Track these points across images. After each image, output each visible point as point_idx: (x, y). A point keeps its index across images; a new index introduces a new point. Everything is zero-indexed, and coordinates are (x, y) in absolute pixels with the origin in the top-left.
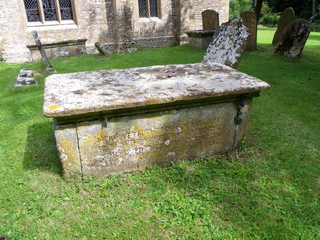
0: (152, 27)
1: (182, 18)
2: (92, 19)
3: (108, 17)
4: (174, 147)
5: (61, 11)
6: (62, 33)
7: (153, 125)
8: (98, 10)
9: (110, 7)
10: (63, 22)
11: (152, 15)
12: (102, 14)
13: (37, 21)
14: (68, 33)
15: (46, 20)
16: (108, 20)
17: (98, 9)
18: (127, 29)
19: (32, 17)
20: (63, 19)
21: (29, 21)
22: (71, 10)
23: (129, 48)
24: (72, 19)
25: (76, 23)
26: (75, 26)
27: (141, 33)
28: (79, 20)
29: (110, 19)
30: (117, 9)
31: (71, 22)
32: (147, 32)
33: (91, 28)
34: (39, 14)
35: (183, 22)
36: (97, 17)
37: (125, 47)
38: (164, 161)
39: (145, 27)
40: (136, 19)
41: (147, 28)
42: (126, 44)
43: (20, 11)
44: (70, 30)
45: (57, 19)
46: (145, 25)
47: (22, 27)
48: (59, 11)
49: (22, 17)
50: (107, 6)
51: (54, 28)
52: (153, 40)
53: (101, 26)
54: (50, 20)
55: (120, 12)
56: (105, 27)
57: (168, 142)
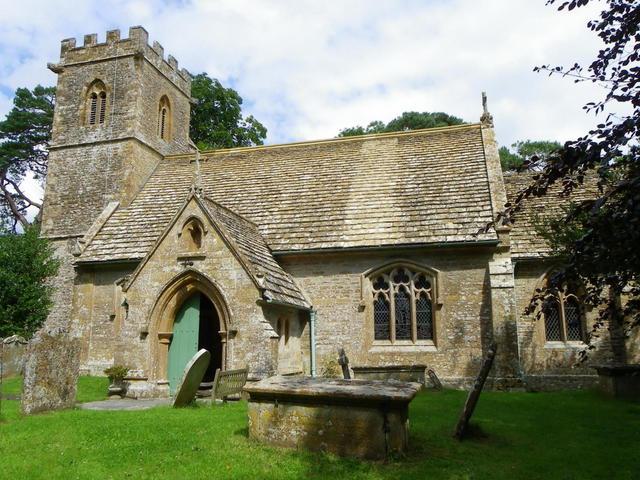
0: (568, 358)
1: (628, 344)
2: (458, 340)
3: (483, 338)
4: (325, 438)
5: (418, 328)
6: (414, 357)
7: (304, 413)
8: (469, 328)
9: (487, 324)
10: (418, 342)
11: (572, 338)
12: (473, 334)
13: (385, 339)
14: (423, 358)
15: (397, 338)
16: (483, 343)
17: (469, 326)
18: (508, 359)
19: (380, 335)
20: (419, 338)
21: (376, 339)
22: (431, 326)
23: (513, 387)
24: (432, 338)
25: (436, 345)
26: (433, 349)
27: (548, 367)
28: (439, 340)
29: (487, 340)
30: (494, 325)
31: (430, 342)
32: (560, 365)
33: (455, 353)
34: (389, 331)
35: (631, 350)
36: (466, 338)
37: (506, 385)
38: (313, 443)
39: (556, 355)
40: (538, 343)
41: (561, 358)
42: (506, 381)
43: (366, 326)
44: (426, 353)
45: (411, 338)
46: (555, 353)
47: (366, 346)
48: (415, 328)
49: (368, 334)
50: (482, 322)
51: (403, 349)
52: (571, 380)
53: (472, 351)
54: (402, 339)
55: (499, 331)
56: (479, 353)
57: (321, 432)
